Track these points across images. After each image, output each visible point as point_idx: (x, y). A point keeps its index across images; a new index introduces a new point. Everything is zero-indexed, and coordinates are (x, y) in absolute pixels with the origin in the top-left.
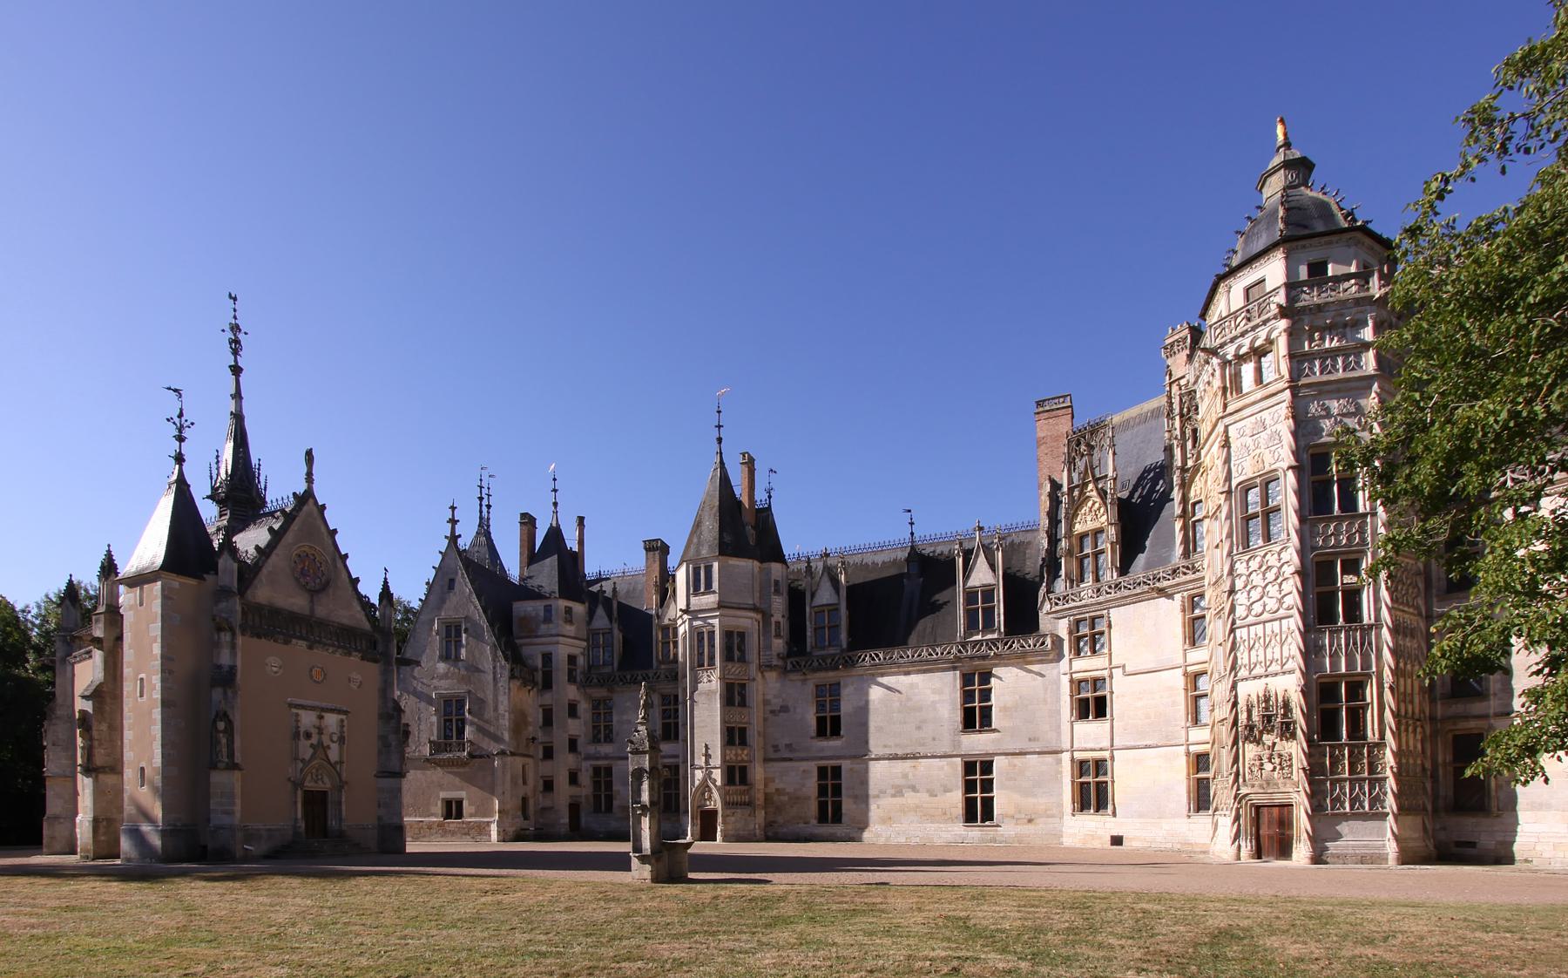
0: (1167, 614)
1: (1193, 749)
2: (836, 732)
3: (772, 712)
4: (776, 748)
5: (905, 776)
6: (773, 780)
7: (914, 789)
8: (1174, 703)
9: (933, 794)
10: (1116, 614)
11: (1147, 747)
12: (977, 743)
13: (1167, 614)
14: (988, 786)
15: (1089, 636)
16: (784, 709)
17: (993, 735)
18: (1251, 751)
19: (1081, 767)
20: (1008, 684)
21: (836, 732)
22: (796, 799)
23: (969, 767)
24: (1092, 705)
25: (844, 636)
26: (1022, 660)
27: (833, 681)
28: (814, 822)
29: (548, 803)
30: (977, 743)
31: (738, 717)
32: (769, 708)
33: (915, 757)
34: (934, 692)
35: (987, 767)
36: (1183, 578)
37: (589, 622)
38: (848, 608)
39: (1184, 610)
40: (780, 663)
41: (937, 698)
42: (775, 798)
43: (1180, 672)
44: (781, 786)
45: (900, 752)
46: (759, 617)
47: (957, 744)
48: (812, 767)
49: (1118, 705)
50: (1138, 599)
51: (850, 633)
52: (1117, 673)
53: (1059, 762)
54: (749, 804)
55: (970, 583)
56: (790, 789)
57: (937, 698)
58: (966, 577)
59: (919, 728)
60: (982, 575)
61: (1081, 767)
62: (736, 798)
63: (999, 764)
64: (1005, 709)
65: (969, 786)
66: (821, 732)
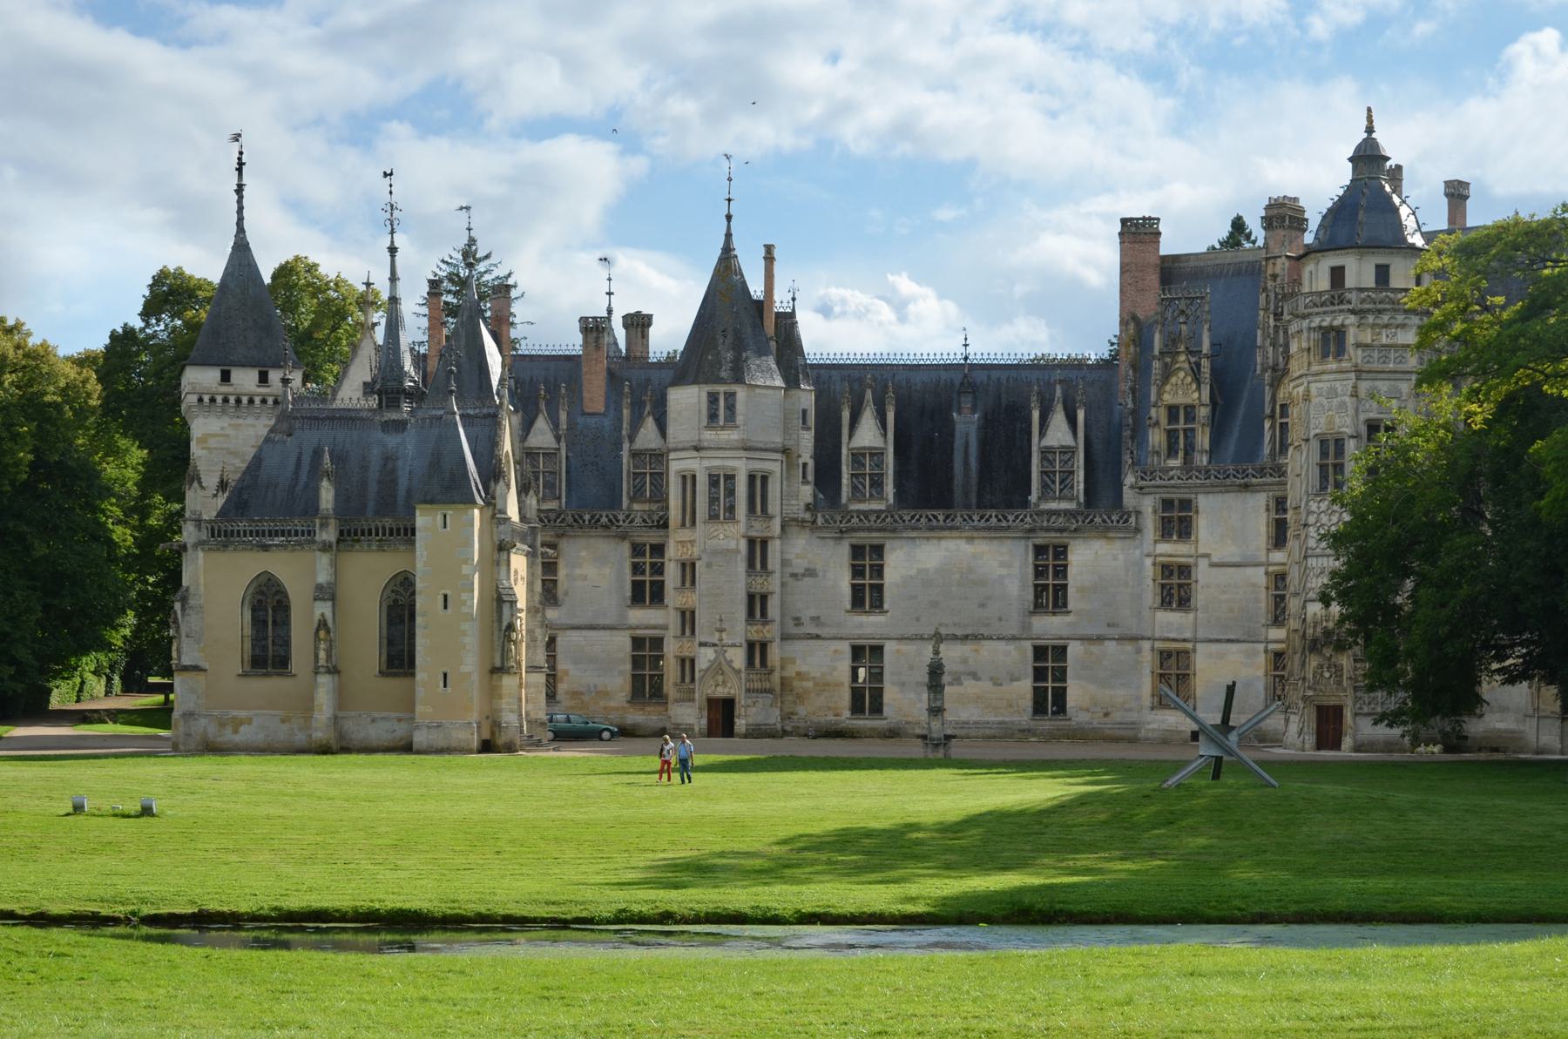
0: (1253, 512)
1: (1271, 646)
2: (878, 605)
3: (794, 575)
4: (798, 622)
5: (965, 661)
6: (793, 661)
7: (975, 676)
8: (1257, 600)
9: (997, 683)
10: (1204, 502)
11: (1229, 641)
12: (1050, 626)
13: (1253, 512)
14: (1061, 675)
15: (1177, 521)
16: (810, 573)
17: (1068, 619)
18: (1314, 661)
19: (1165, 656)
20: (1088, 559)
21: (878, 605)
22: (824, 686)
23: (1040, 653)
24: (1175, 587)
25: (889, 489)
26: (1104, 532)
27: (876, 542)
28: (847, 713)
29: (938, 704)
30: (1050, 626)
31: (759, 585)
32: (789, 570)
33: (976, 638)
34: (1002, 564)
35: (1061, 652)
36: (1269, 479)
37: (524, 438)
38: (895, 486)
39: (1268, 510)
40: (808, 516)
41: (1004, 572)
42: (796, 683)
43: (1262, 570)
44: (804, 669)
45: (959, 633)
46: (778, 456)
47: (1026, 626)
48: (845, 647)
49: (1200, 596)
50: (1227, 489)
51: (898, 485)
52: (1203, 564)
53: (1139, 651)
54: (770, 691)
55: (1045, 443)
56: (816, 673)
57: (1004, 572)
58: (1042, 434)
59: (982, 605)
60: (1059, 433)
61: (1165, 656)
62: (758, 685)
63: (1074, 649)
64: (1082, 590)
65: (1039, 674)
66: (858, 601)
